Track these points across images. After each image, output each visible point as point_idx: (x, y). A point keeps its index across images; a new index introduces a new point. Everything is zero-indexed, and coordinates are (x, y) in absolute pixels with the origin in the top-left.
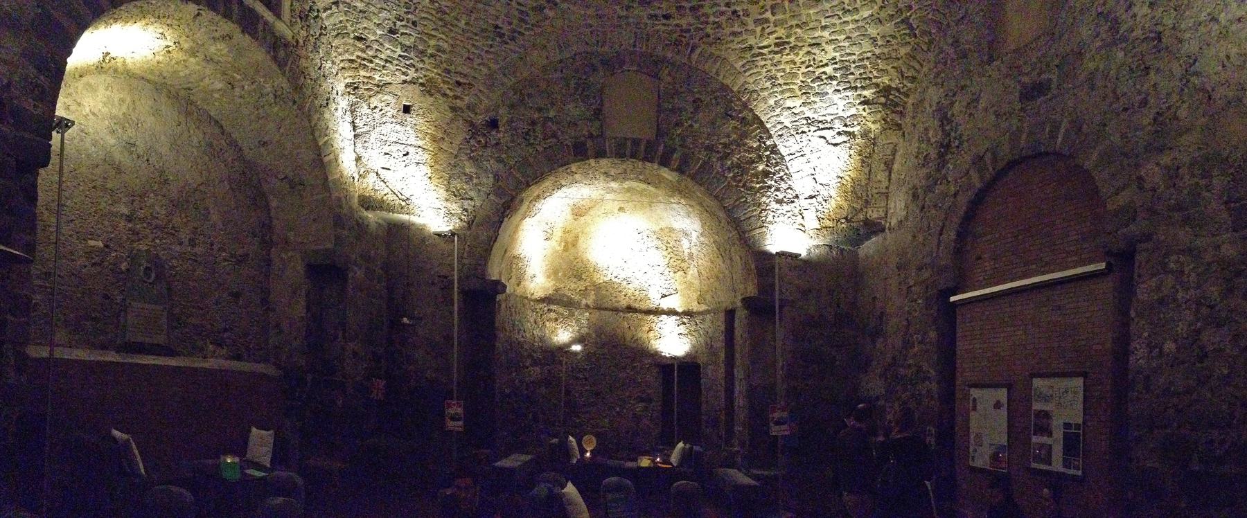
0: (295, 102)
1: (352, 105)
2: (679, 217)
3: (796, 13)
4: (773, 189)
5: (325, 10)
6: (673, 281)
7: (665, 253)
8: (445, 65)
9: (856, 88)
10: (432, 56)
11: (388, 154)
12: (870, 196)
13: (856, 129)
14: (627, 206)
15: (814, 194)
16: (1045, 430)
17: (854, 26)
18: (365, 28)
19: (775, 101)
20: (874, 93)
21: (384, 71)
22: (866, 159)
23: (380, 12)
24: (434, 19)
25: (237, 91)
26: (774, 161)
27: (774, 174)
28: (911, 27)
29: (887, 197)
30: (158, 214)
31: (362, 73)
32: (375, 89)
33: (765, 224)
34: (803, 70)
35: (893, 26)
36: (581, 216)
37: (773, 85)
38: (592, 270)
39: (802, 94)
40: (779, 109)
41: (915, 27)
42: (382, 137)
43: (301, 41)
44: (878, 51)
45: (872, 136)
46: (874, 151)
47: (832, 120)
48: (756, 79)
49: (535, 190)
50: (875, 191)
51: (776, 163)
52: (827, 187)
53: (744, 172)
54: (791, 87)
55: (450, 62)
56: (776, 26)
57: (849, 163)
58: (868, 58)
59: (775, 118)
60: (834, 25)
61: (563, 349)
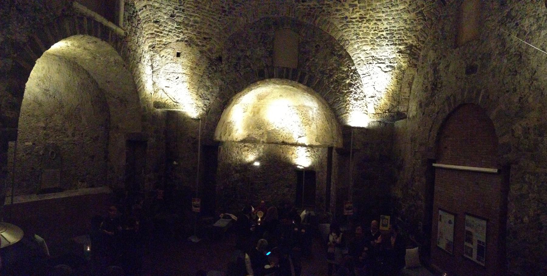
0: (124, 66)
1: (151, 57)
2: (307, 101)
3: (370, 4)
4: (353, 93)
5: (140, 10)
6: (304, 130)
7: (301, 116)
8: (198, 30)
9: (396, 44)
10: (192, 26)
11: (168, 79)
12: (400, 99)
13: (395, 65)
14: (284, 95)
15: (373, 95)
16: (470, 240)
17: (396, 13)
18: (159, 16)
19: (358, 46)
20: (404, 48)
21: (168, 37)
22: (399, 81)
23: (166, 7)
24: (193, 7)
25: (97, 60)
26: (355, 78)
27: (354, 85)
28: (423, 16)
29: (409, 101)
30: (58, 124)
31: (157, 39)
32: (163, 46)
33: (348, 112)
34: (372, 32)
35: (415, 15)
36: (262, 99)
37: (357, 38)
38: (266, 124)
39: (371, 44)
40: (360, 51)
41: (425, 15)
42: (166, 71)
43: (128, 33)
44: (407, 27)
45: (403, 69)
46: (403, 77)
47: (385, 59)
48: (349, 34)
49: (239, 94)
50: (403, 97)
51: (355, 79)
52: (380, 93)
53: (339, 84)
54: (366, 39)
55: (201, 28)
56: (360, 9)
57: (391, 82)
58: (402, 30)
59: (357, 55)
60: (387, 12)
61: (250, 164)
